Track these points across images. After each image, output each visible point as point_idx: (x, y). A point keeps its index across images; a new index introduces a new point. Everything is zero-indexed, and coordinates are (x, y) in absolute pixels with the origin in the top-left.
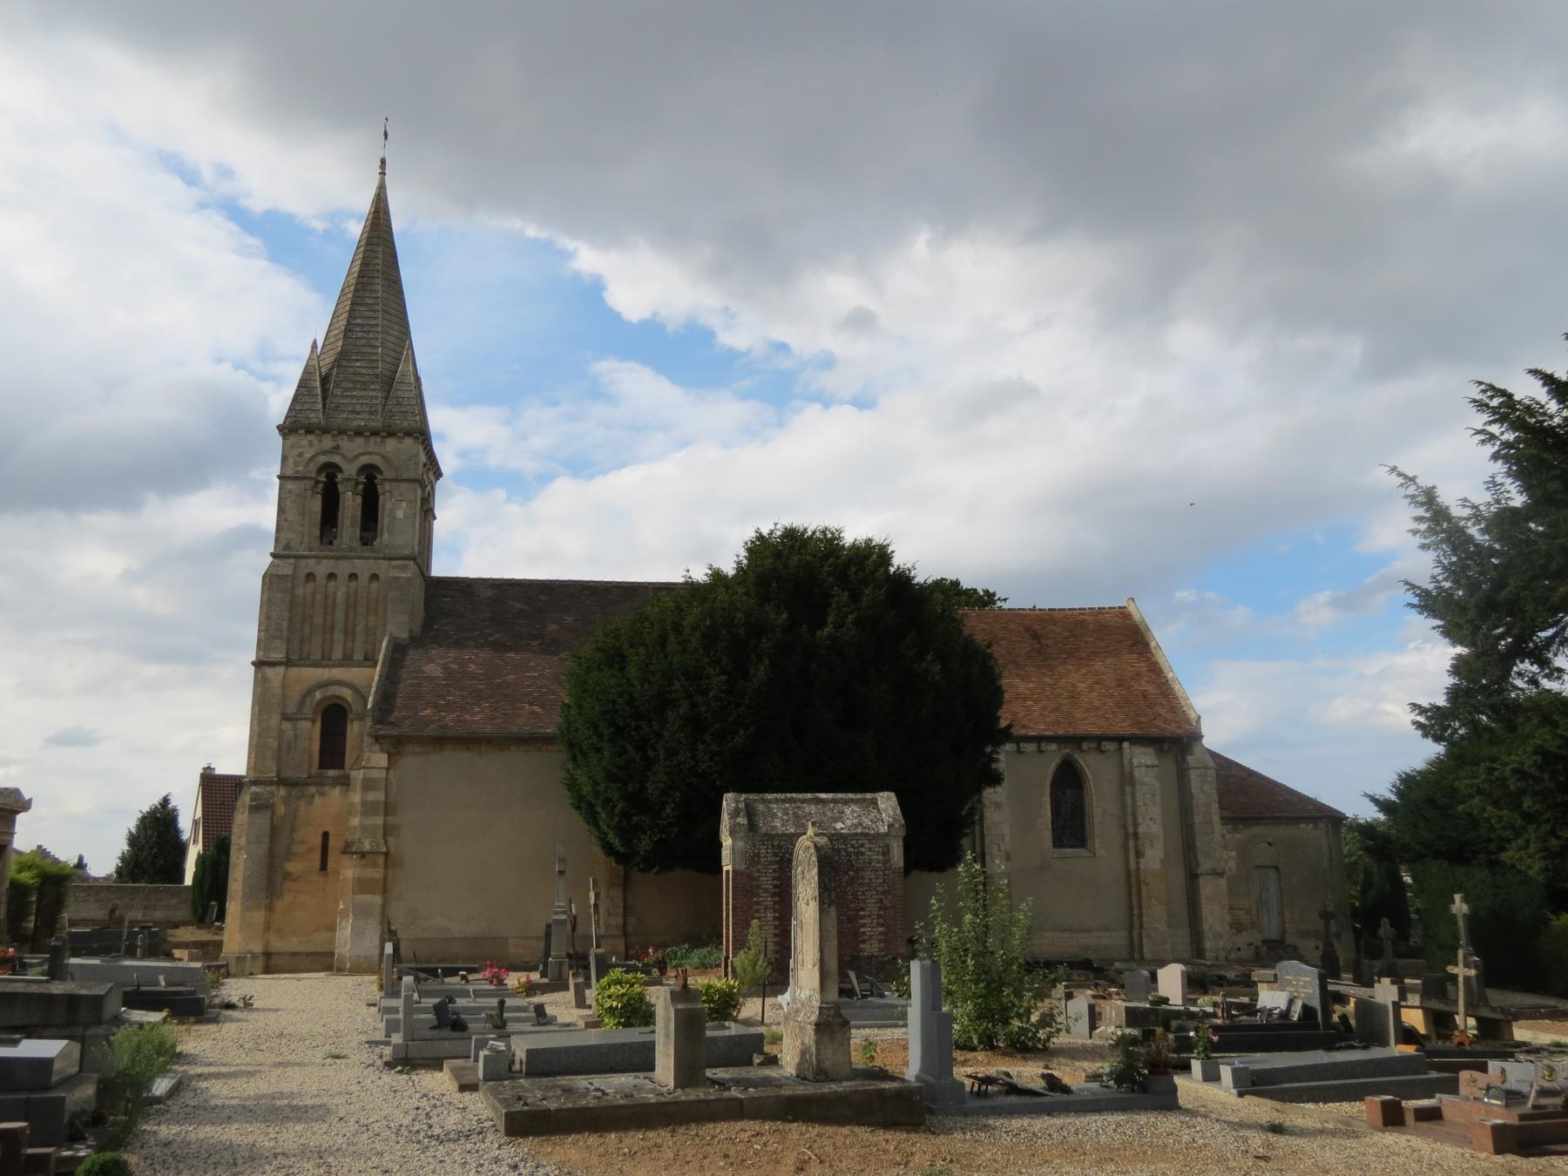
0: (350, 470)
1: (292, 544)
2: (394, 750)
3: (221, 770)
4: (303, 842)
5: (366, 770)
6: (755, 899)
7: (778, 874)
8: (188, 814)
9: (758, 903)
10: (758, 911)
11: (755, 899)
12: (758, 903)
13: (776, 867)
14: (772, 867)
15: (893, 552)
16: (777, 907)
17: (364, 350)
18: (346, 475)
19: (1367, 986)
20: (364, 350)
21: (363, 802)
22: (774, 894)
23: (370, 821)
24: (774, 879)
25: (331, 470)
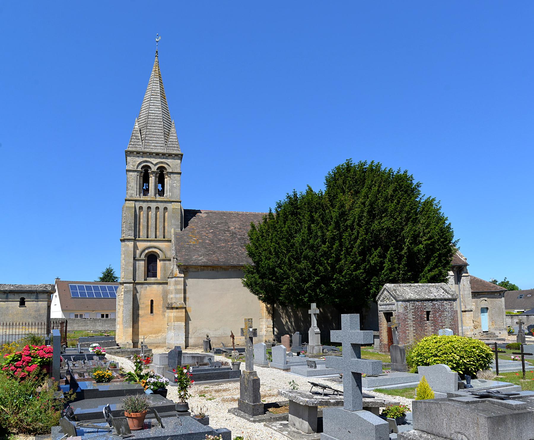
0: (154, 169)
1: (133, 195)
2: (185, 270)
3: (19, 305)
4: (143, 303)
5: (177, 279)
6: (407, 323)
7: (414, 314)
8: (83, 354)
9: (408, 324)
10: (408, 327)
11: (407, 323)
12: (408, 324)
13: (413, 311)
14: (412, 311)
15: (418, 185)
16: (414, 325)
17: (156, 123)
18: (153, 170)
19: (529, 326)
20: (156, 123)
21: (175, 289)
22: (414, 321)
23: (178, 296)
24: (413, 315)
25: (146, 169)
